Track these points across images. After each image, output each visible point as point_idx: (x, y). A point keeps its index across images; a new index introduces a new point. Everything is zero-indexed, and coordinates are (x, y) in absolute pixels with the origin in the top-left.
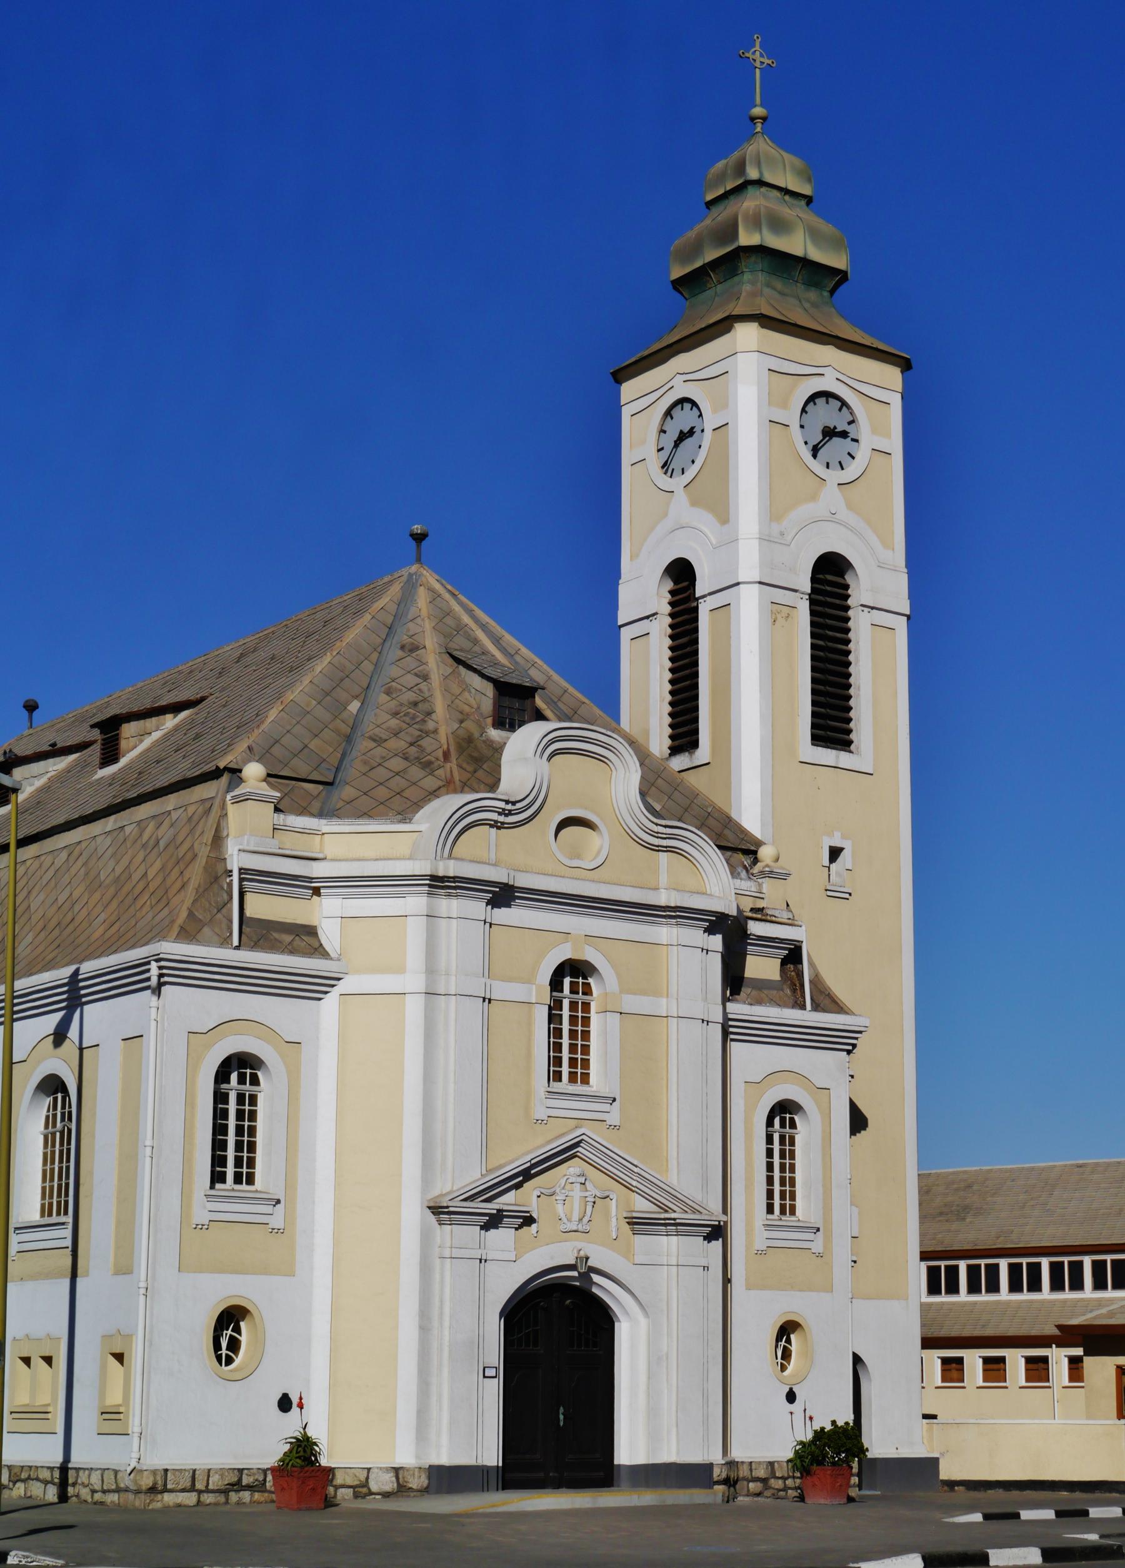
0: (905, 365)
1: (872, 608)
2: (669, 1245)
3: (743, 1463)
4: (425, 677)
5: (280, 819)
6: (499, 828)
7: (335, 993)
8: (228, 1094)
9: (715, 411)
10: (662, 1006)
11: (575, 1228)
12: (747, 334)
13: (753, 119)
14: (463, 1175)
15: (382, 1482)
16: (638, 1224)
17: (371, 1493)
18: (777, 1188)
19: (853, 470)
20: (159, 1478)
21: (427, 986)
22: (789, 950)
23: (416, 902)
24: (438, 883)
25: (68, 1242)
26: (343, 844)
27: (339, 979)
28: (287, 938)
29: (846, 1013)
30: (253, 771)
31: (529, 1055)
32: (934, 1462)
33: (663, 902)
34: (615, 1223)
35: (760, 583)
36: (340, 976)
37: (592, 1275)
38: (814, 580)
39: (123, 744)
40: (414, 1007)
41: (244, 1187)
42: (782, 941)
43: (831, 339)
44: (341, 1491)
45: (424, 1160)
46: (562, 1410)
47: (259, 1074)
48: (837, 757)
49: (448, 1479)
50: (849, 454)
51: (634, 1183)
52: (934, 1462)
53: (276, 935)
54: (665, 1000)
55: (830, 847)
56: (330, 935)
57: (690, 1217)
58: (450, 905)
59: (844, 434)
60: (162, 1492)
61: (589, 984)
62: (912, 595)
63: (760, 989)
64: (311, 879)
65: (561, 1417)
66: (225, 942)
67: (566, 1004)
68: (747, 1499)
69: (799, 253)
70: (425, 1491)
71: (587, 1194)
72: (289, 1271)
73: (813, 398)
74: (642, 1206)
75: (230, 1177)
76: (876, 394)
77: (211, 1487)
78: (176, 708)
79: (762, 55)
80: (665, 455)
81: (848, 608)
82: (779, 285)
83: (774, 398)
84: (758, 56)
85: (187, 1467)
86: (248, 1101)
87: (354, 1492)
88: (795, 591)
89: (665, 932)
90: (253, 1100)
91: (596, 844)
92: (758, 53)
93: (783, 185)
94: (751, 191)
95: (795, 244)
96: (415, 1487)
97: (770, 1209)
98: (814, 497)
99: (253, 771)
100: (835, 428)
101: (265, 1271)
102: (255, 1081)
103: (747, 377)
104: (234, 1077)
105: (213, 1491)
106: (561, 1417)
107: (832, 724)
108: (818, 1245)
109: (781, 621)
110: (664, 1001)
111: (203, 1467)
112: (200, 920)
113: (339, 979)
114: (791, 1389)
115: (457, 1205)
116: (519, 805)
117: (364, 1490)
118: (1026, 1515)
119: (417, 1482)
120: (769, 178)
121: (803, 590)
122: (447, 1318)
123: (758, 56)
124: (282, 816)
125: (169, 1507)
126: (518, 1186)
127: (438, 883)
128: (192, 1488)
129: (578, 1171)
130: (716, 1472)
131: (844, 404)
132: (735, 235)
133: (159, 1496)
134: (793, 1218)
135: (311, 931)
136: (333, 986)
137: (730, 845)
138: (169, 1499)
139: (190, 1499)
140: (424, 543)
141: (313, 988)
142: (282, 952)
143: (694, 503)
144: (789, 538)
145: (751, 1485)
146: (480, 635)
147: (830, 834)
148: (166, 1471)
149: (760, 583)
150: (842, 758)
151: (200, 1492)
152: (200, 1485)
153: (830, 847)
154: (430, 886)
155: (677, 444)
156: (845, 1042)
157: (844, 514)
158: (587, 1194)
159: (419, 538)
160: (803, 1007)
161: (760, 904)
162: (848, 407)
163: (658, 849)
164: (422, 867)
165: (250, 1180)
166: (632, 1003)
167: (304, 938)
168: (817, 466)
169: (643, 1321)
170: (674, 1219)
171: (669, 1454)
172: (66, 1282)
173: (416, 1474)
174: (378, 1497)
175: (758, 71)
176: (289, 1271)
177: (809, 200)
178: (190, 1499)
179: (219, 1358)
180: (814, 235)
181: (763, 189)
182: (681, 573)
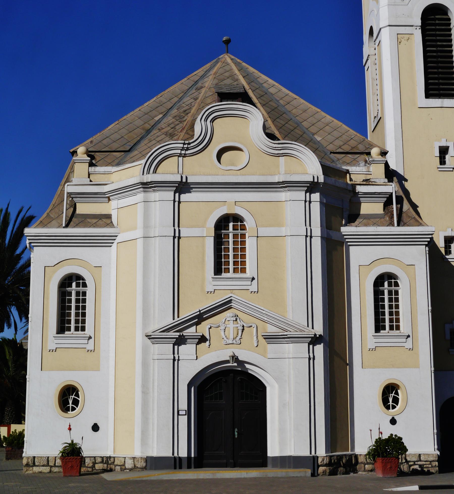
2: (289, 349)
3: (360, 455)
5: (92, 169)
6: (183, 157)
8: (71, 292)
10: (283, 231)
11: (231, 342)
15: (129, 464)
16: (271, 338)
17: (126, 469)
20: (30, 460)
22: (176, 187)
23: (140, 196)
27: (117, 236)
28: (94, 221)
29: (423, 226)
33: (276, 180)
35: (389, 26)
36: (116, 235)
40: (140, 242)
41: (80, 332)
42: (380, 193)
45: (143, 314)
46: (236, 430)
48: (442, 102)
49: (153, 463)
51: (266, 319)
53: (89, 220)
55: (439, 146)
57: (298, 334)
58: (155, 195)
60: (32, 466)
61: (244, 225)
63: (369, 219)
64: (104, 193)
65: (236, 433)
66: (60, 226)
67: (231, 236)
68: (364, 473)
70: (145, 468)
71: (237, 325)
74: (271, 330)
77: (57, 465)
85: (45, 456)
86: (394, 297)
87: (121, 468)
88: (412, 26)
89: (284, 195)
91: (242, 158)
96: (139, 466)
101: (85, 369)
102: (397, 285)
104: (386, 284)
105: (58, 466)
106: (236, 433)
108: (90, 346)
109: (404, 42)
110: (283, 229)
111: (52, 456)
112: (52, 218)
113: (117, 236)
114: (393, 418)
115: (158, 334)
116: (192, 145)
117: (123, 467)
121: (416, 25)
124: (93, 168)
125: (36, 473)
126: (197, 324)
128: (48, 465)
130: (320, 460)
133: (31, 468)
135: (109, 217)
136: (115, 240)
138: (36, 469)
139: (46, 470)
140: (229, 45)
141: (106, 242)
142: (90, 227)
145: (366, 466)
147: (439, 141)
149: (389, 26)
151: (51, 467)
152: (51, 464)
153: (439, 146)
154: (143, 188)
158: (237, 325)
159: (227, 42)
160: (393, 225)
161: (368, 177)
163: (278, 155)
165: (398, 328)
167: (105, 219)
170: (287, 335)
171: (291, 451)
174: (128, 471)
176: (96, 368)
178: (46, 470)
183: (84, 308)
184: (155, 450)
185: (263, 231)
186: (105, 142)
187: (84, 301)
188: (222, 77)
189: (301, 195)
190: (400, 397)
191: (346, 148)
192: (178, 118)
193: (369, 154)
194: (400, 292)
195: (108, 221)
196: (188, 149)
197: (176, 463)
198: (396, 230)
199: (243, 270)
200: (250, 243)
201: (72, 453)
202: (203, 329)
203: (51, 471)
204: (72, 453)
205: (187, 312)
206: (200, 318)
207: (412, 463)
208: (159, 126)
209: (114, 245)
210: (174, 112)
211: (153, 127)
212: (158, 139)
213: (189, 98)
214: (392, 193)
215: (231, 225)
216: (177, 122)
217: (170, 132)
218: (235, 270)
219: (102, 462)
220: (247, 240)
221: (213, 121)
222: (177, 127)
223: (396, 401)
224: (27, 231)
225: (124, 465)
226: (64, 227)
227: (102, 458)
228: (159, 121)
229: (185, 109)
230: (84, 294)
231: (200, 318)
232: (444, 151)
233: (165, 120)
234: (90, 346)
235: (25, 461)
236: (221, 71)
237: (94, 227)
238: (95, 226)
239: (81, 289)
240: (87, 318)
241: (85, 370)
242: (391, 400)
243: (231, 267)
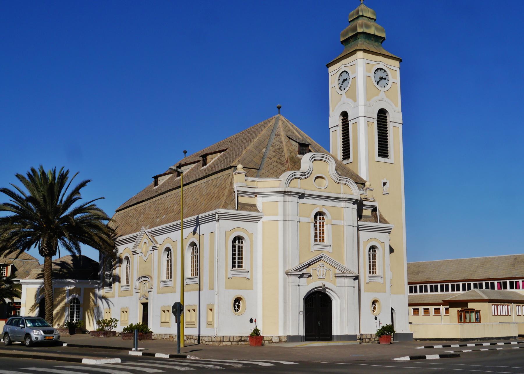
0: (400, 61)
2: (345, 282)
4: (281, 142)
5: (246, 178)
7: (261, 221)
9: (352, 74)
10: (342, 222)
12: (360, 54)
14: (294, 265)
15: (276, 340)
16: (337, 276)
18: (371, 267)
23: (281, 198)
24: (286, 193)
25: (198, 282)
26: (262, 184)
28: (249, 207)
30: (240, 166)
32: (412, 334)
34: (332, 276)
38: (378, 115)
39: (208, 161)
40: (281, 224)
42: (372, 206)
52: (412, 334)
56: (259, 207)
57: (350, 275)
58: (289, 199)
59: (385, 79)
62: (403, 119)
69: (373, 33)
70: (286, 341)
73: (377, 70)
74: (338, 272)
76: (393, 69)
78: (220, 151)
80: (340, 85)
81: (387, 122)
82: (368, 41)
83: (367, 70)
89: (342, 204)
90: (242, 247)
91: (324, 183)
94: (360, 18)
97: (370, 272)
98: (378, 95)
99: (240, 166)
101: (246, 289)
102: (242, 243)
103: (360, 65)
104: (237, 242)
108: (382, 281)
109: (370, 126)
118: (435, 347)
119: (284, 339)
120: (365, 15)
126: (307, 267)
127: (286, 193)
128: (230, 341)
130: (358, 337)
131: (385, 71)
132: (356, 29)
135: (255, 206)
139: (229, 343)
143: (347, 97)
146: (295, 131)
152: (231, 340)
155: (343, 82)
156: (388, 231)
157: (385, 99)
159: (279, 108)
160: (377, 222)
161: (366, 197)
163: (340, 183)
164: (282, 189)
166: (334, 222)
167: (253, 207)
169: (339, 300)
171: (346, 332)
172: (198, 292)
176: (251, 288)
177: (375, 20)
178: (229, 343)
179: (235, 310)
180: (376, 28)
182: (345, 115)
184: (290, 332)
190: (241, 305)
194: (377, 255)
196: (303, 175)
223: (239, 307)
225: (271, 340)
234: (248, 276)
238: (246, 210)
241: (246, 289)
242: (236, 306)
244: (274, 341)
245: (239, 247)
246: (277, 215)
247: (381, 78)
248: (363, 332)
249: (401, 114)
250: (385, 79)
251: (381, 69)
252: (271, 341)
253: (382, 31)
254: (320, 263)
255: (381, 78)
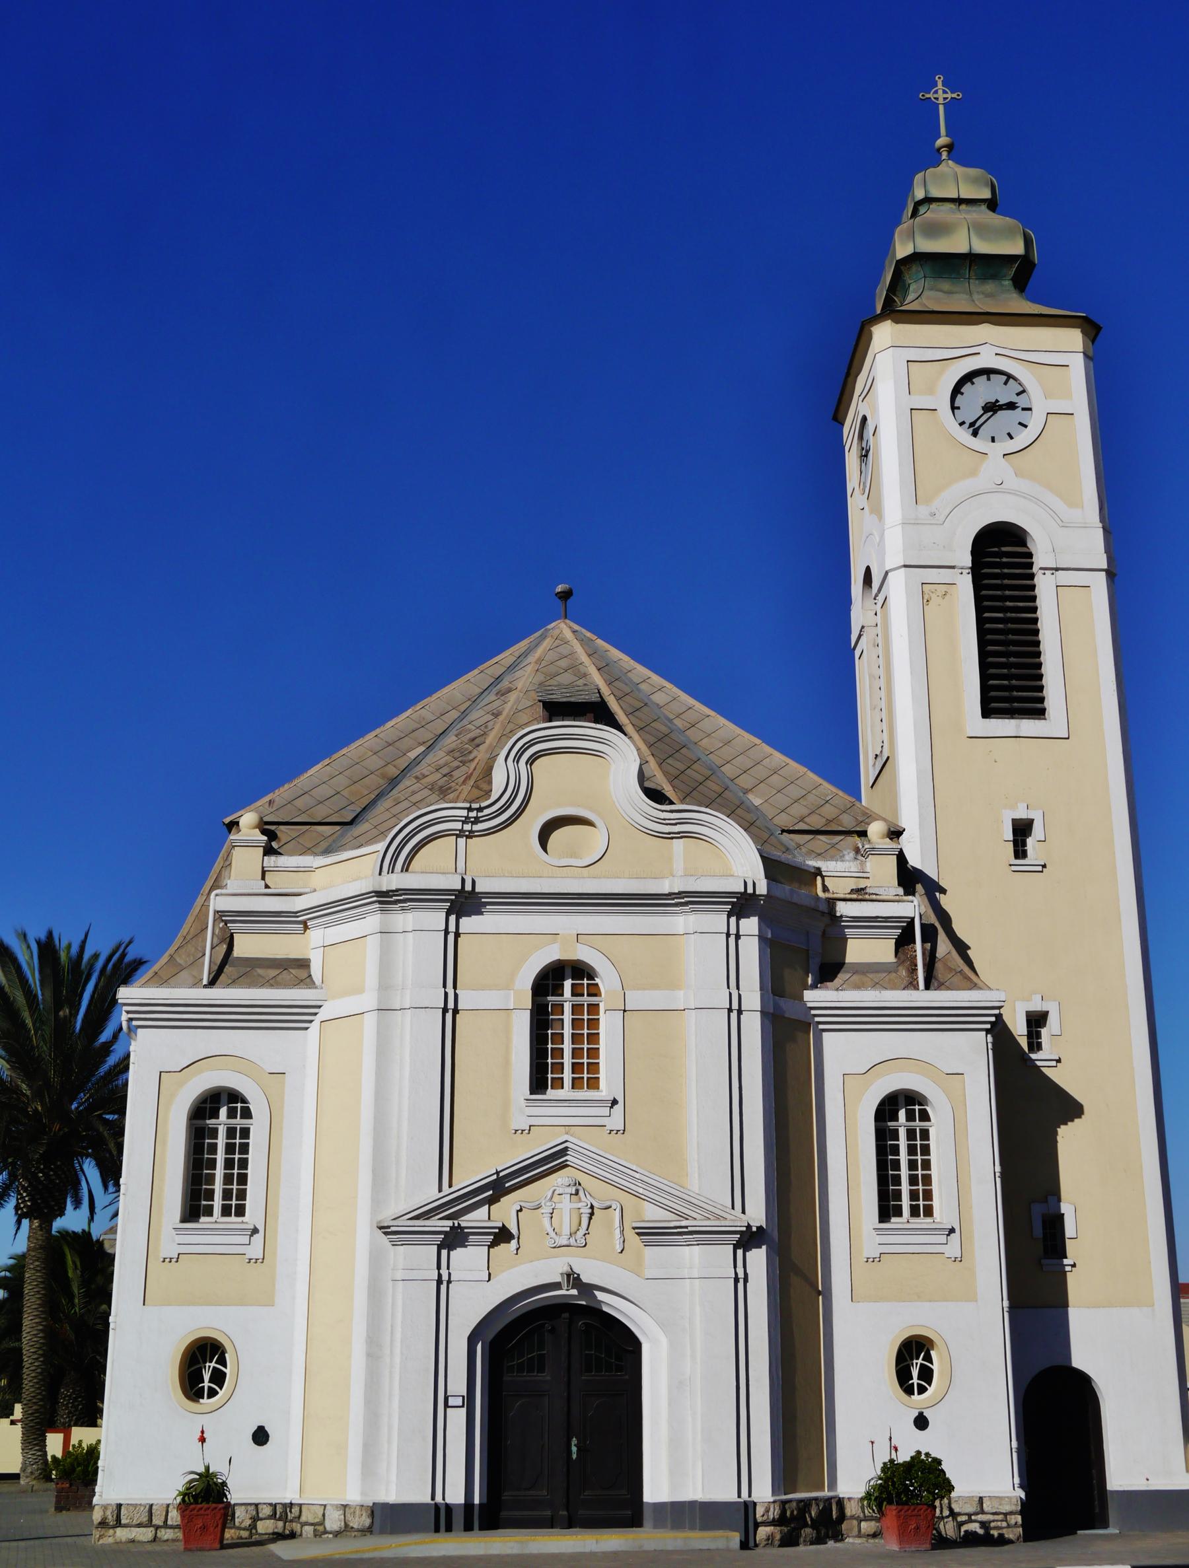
1: (1057, 569)
3: (849, 1499)
10: (680, 999)
11: (565, 1242)
13: (938, 150)
15: (334, 1522)
16: (651, 1234)
17: (325, 1532)
19: (1023, 438)
20: (108, 1513)
21: (379, 1002)
23: (372, 921)
24: (386, 898)
27: (320, 1007)
28: (272, 973)
31: (506, 1063)
35: (905, 566)
36: (319, 1003)
37: (597, 1293)
40: (370, 1021)
41: (233, 1219)
43: (983, 317)
44: (306, 1528)
46: (574, 1441)
47: (928, 1109)
48: (1018, 726)
50: (1020, 424)
51: (641, 1191)
53: (260, 971)
54: (682, 992)
59: (1011, 406)
60: (114, 1527)
62: (1108, 550)
63: (864, 973)
65: (574, 1449)
66: (196, 984)
67: (567, 1008)
68: (858, 1541)
69: (963, 249)
70: (369, 1530)
72: (267, 1299)
74: (654, 1215)
75: (217, 1210)
76: (1053, 366)
79: (945, 92)
81: (1032, 577)
82: (946, 285)
84: (941, 94)
85: (143, 1502)
86: (920, 1144)
88: (953, 567)
89: (681, 921)
90: (925, 1134)
91: (593, 841)
92: (940, 92)
93: (955, 196)
95: (957, 243)
96: (355, 1526)
98: (973, 473)
100: (997, 401)
101: (242, 1301)
102: (925, 1116)
104: (902, 1114)
105: (172, 1527)
106: (574, 1449)
107: (1011, 679)
108: (255, 1250)
109: (935, 599)
110: (681, 993)
113: (320, 1007)
114: (921, 1414)
116: (486, 812)
117: (321, 1528)
119: (361, 1521)
120: (935, 193)
122: (398, 1344)
123: (941, 94)
124: (273, 858)
126: (492, 1201)
127: (386, 898)
128: (149, 1523)
129: (566, 1181)
130: (760, 1511)
131: (1009, 377)
133: (111, 1531)
134: (929, 1220)
135: (304, 964)
136: (316, 1014)
137: (840, 829)
138: (122, 1534)
141: (297, 1018)
142: (262, 986)
144: (942, 518)
145: (863, 1524)
147: (1013, 807)
148: (119, 1506)
149: (905, 566)
150: (1028, 726)
151: (157, 1528)
152: (157, 1521)
154: (380, 902)
157: (1012, 482)
158: (580, 1205)
159: (566, 596)
160: (916, 988)
161: (862, 884)
162: (1015, 379)
163: (670, 836)
167: (296, 970)
168: (977, 443)
171: (695, 1491)
173: (358, 1512)
175: (941, 108)
178: (146, 1534)
180: (981, 230)
181: (934, 206)
183: (244, 1164)
184: (393, 1487)
185: (635, 999)
186: (299, 803)
187: (245, 1148)
188: (552, 669)
189: (718, 920)
190: (935, 1367)
191: (816, 822)
192: (457, 754)
193: (863, 834)
195: (302, 974)
196: (477, 821)
197: (440, 1518)
198: (922, 997)
199: (594, 1084)
200: (608, 1025)
201: (206, 1496)
202: (504, 1212)
203: (155, 1539)
204: (206, 1496)
205: (472, 1172)
206: (497, 1188)
207: (964, 1518)
208: (417, 771)
209: (314, 1027)
210: (450, 741)
211: (404, 772)
212: (414, 799)
213: (481, 712)
214: (913, 919)
215: (568, 984)
216: (456, 763)
217: (441, 783)
218: (576, 1084)
219: (273, 1516)
220: (603, 1017)
221: (531, 761)
222: (456, 774)
223: (926, 1375)
224: (125, 994)
226: (205, 986)
227: (274, 1506)
228: (417, 761)
229: (472, 735)
230: (245, 1133)
231: (497, 1188)
232: (1022, 830)
233: (430, 759)
234: (255, 1250)
235: (97, 1516)
236: (551, 656)
237: (272, 986)
238: (272, 983)
239: (239, 1122)
240: (250, 1187)
242: (915, 1373)
243: (567, 1075)
244: (328, 1529)
245: (911, 1134)
246: (359, 990)
247: (992, 408)
248: (448, 1501)
249: (1099, 533)
250: (1011, 406)
251: (988, 372)
252: (320, 1530)
253: (1007, 233)
254: (559, 1180)
255: (992, 408)
